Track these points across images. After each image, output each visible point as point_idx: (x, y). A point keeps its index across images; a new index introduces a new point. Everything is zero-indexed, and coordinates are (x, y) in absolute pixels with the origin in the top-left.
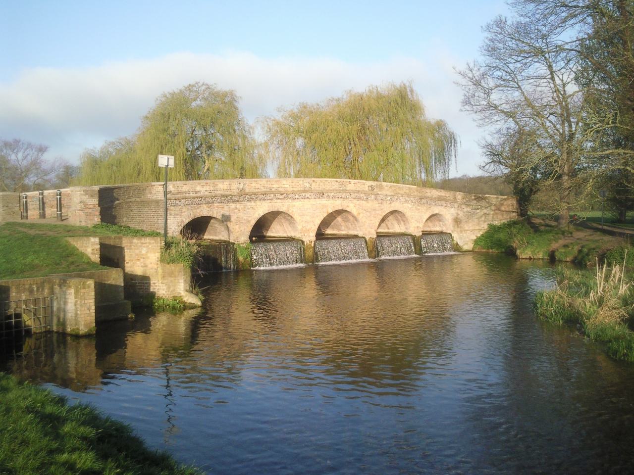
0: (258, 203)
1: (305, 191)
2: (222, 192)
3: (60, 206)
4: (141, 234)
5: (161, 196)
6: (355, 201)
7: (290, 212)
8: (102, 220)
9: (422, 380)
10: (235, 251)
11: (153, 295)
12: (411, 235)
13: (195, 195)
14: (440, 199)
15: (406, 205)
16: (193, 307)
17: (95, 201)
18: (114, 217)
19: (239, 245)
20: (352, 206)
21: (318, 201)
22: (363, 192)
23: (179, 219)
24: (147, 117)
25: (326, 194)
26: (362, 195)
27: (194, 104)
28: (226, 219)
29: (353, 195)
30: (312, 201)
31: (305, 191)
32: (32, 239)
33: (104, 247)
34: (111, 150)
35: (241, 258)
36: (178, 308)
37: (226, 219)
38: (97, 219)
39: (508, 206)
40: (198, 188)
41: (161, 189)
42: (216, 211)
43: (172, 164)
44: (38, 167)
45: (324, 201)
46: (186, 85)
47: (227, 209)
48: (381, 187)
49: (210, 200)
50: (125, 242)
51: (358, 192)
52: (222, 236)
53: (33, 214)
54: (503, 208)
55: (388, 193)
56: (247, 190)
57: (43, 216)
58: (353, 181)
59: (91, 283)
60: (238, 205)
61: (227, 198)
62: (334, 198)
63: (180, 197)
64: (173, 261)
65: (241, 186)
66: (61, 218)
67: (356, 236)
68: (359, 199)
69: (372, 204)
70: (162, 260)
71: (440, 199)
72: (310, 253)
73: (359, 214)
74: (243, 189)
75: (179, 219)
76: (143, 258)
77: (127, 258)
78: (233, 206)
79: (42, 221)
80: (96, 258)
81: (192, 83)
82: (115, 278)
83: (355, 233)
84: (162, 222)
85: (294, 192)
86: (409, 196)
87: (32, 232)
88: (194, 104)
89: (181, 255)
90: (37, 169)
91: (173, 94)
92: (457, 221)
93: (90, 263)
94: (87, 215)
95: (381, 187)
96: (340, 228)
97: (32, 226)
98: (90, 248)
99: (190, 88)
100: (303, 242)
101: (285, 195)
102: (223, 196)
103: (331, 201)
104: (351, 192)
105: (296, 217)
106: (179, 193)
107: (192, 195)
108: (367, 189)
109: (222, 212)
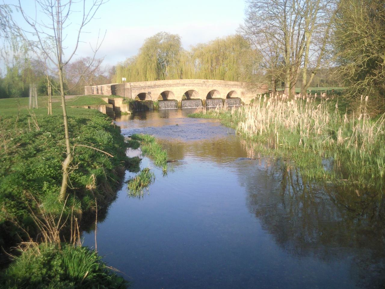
0: (161, 88)
1: (177, 84)
2: (148, 85)
3: (102, 90)
4: (120, 97)
5: (129, 87)
6: (197, 87)
7: (172, 91)
8: (112, 94)
9: (2, 54)
10: (153, 103)
11: (121, 111)
12: (222, 99)
13: (140, 86)
14: (235, 85)
15: (219, 88)
16: (129, 114)
17: (110, 89)
18: (116, 93)
19: (154, 102)
20: (195, 88)
21: (182, 87)
22: (201, 84)
23: (135, 94)
24: (141, 49)
25: (185, 85)
26: (200, 85)
27: (161, 41)
28: (149, 93)
29: (196, 85)
30: (180, 87)
31: (177, 84)
32: (94, 98)
33: (109, 100)
34: (129, 62)
35: (155, 106)
36: (126, 114)
37: (149, 93)
38: (111, 94)
39: (264, 87)
40: (141, 84)
41: (129, 85)
42: (146, 91)
43: (125, 80)
44: (98, 69)
45: (185, 87)
46: (157, 33)
47: (150, 90)
48: (208, 82)
49: (144, 88)
50: (115, 99)
51: (198, 83)
52: (150, 99)
53: (95, 92)
54: (262, 88)
55: (211, 84)
56: (157, 84)
57: (98, 93)
58: (196, 80)
59: (105, 106)
60: (154, 89)
61: (149, 87)
62: (189, 86)
63: (135, 87)
64: (125, 103)
65: (155, 83)
66: (102, 93)
67: (199, 99)
68: (199, 86)
69: (204, 87)
70: (123, 103)
71: (235, 85)
72: (180, 105)
73: (199, 91)
74: (155, 84)
75: (135, 94)
76: (119, 103)
77: (115, 103)
78: (152, 89)
79: (98, 94)
80: (107, 102)
81: (159, 32)
82: (111, 106)
83: (198, 98)
84: (130, 94)
85: (173, 84)
86: (220, 84)
87: (94, 97)
88: (161, 41)
89: (126, 102)
90: (98, 71)
91: (151, 38)
92: (243, 93)
93: (106, 103)
94: (108, 93)
95: (208, 82)
96: (233, 96)
97: (94, 95)
98: (106, 100)
99: (158, 35)
100: (177, 101)
101: (170, 85)
102: (148, 86)
103: (188, 87)
104: (195, 84)
105: (174, 92)
106: (135, 86)
107: (139, 86)
108: (202, 82)
109: (149, 91)
